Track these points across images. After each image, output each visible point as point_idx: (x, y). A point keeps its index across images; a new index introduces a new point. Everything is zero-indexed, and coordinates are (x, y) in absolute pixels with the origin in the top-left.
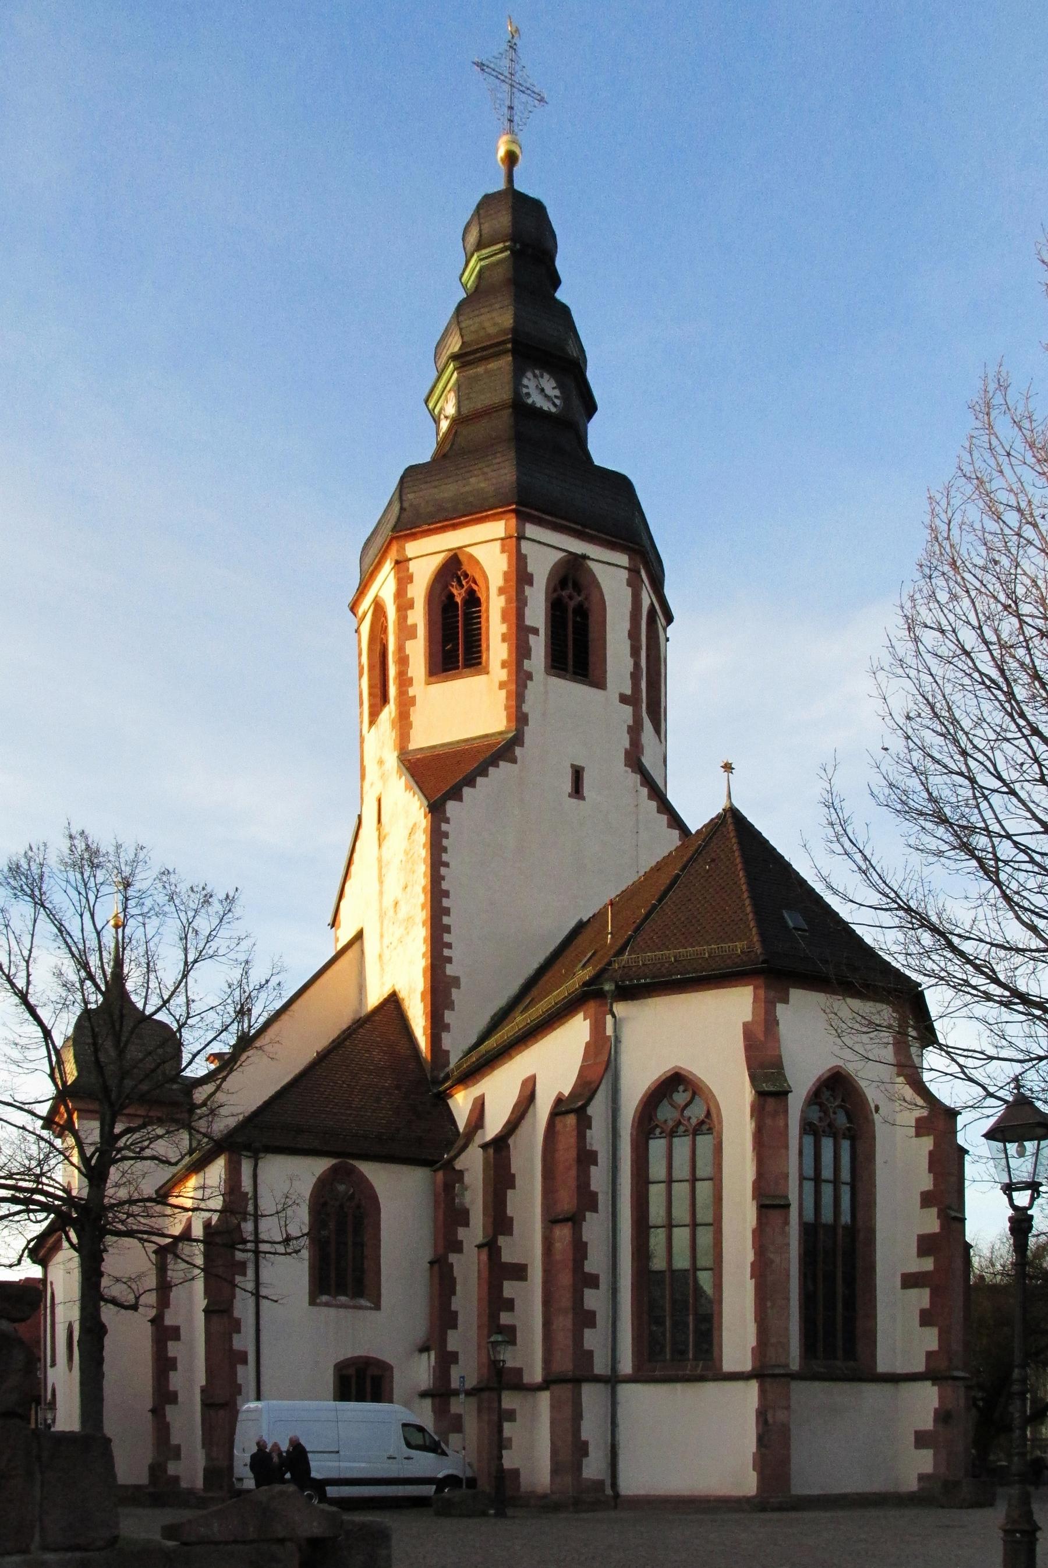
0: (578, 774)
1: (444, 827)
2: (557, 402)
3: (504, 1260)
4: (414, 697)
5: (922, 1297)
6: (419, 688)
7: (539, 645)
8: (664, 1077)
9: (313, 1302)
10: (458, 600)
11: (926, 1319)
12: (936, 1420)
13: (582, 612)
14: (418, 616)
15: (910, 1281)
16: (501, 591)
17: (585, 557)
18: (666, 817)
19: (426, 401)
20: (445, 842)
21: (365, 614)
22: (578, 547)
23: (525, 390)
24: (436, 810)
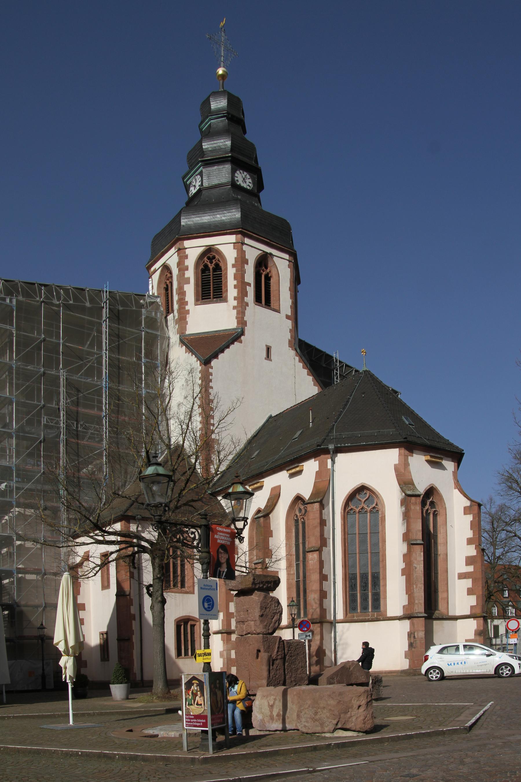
0: (268, 349)
1: (210, 370)
2: (250, 185)
5: (468, 583)
7: (251, 291)
8: (357, 487)
10: (211, 268)
11: (470, 592)
12: (475, 635)
13: (268, 278)
14: (190, 274)
15: (462, 576)
16: (233, 266)
17: (271, 254)
18: (306, 370)
19: (183, 178)
21: (155, 271)
22: (268, 250)
24: (206, 362)
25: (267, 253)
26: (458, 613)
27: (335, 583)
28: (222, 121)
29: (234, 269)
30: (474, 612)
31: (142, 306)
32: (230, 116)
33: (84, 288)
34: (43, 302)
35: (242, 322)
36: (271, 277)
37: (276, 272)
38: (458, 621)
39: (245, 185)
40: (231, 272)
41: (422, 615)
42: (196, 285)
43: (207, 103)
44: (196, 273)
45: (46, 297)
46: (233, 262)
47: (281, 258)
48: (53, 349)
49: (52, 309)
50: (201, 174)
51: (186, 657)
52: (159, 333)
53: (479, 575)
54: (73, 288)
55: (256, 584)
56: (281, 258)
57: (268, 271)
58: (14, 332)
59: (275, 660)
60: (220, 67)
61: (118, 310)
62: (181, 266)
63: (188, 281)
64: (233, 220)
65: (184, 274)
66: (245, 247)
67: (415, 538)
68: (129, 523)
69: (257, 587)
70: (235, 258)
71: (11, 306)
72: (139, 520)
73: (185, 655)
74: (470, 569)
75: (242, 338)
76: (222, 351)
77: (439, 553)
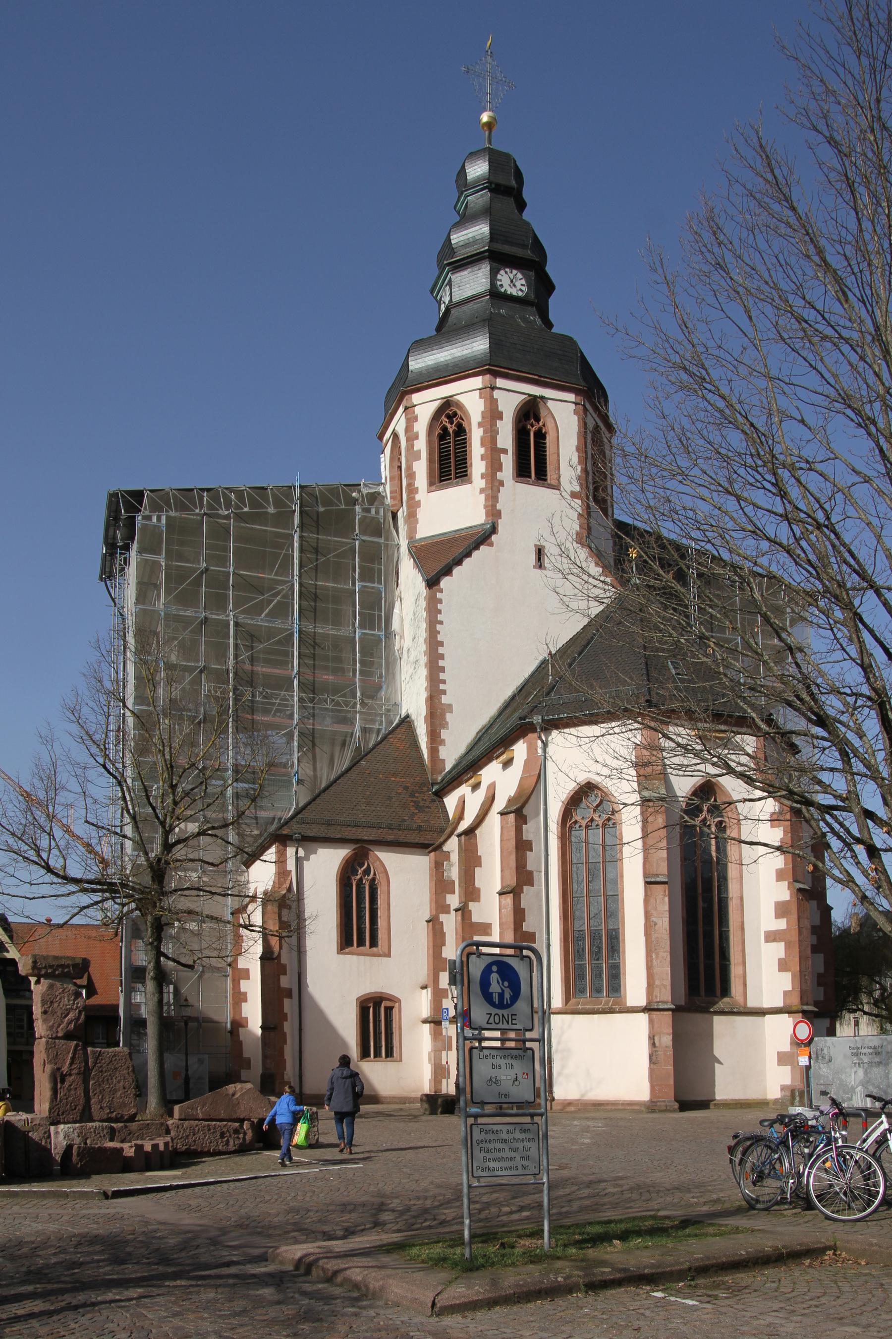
1: (439, 595)
2: (523, 288)
3: (473, 920)
4: (419, 501)
6: (423, 494)
7: (508, 461)
9: (388, 955)
10: (451, 431)
13: (541, 436)
14: (421, 445)
15: (772, 937)
16: (480, 425)
17: (542, 398)
19: (432, 292)
20: (439, 606)
23: (499, 283)
24: (432, 583)
25: (535, 397)
26: (766, 1004)
27: (549, 945)
28: (482, 196)
29: (481, 429)
30: (788, 1002)
31: (355, 502)
32: (493, 186)
33: (265, 485)
34: (205, 514)
35: (494, 513)
36: (546, 433)
37: (553, 425)
38: (767, 1016)
39: (513, 291)
40: (476, 435)
41: (666, 1007)
42: (430, 460)
43: (462, 172)
44: (430, 443)
45: (210, 507)
46: (480, 419)
47: (561, 401)
48: (219, 583)
49: (218, 523)
50: (450, 283)
51: (388, 1059)
52: (382, 540)
53: (795, 937)
54: (250, 488)
55: (40, 969)
56: (561, 401)
57: (541, 424)
58: (163, 564)
59: (66, 1075)
60: (485, 110)
61: (318, 512)
62: (409, 434)
63: (417, 456)
64: (475, 353)
65: (413, 446)
66: (496, 394)
67: (655, 872)
68: (285, 846)
69: (43, 972)
70: (482, 412)
71: (159, 527)
72: (297, 840)
73: (375, 1056)
74: (781, 924)
75: (494, 538)
76: (459, 562)
77: (730, 895)
